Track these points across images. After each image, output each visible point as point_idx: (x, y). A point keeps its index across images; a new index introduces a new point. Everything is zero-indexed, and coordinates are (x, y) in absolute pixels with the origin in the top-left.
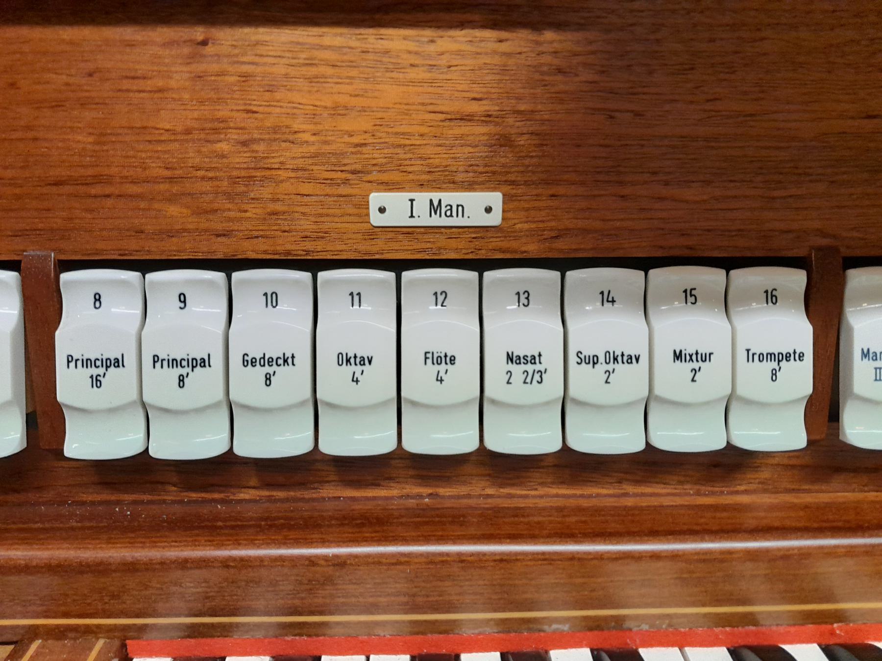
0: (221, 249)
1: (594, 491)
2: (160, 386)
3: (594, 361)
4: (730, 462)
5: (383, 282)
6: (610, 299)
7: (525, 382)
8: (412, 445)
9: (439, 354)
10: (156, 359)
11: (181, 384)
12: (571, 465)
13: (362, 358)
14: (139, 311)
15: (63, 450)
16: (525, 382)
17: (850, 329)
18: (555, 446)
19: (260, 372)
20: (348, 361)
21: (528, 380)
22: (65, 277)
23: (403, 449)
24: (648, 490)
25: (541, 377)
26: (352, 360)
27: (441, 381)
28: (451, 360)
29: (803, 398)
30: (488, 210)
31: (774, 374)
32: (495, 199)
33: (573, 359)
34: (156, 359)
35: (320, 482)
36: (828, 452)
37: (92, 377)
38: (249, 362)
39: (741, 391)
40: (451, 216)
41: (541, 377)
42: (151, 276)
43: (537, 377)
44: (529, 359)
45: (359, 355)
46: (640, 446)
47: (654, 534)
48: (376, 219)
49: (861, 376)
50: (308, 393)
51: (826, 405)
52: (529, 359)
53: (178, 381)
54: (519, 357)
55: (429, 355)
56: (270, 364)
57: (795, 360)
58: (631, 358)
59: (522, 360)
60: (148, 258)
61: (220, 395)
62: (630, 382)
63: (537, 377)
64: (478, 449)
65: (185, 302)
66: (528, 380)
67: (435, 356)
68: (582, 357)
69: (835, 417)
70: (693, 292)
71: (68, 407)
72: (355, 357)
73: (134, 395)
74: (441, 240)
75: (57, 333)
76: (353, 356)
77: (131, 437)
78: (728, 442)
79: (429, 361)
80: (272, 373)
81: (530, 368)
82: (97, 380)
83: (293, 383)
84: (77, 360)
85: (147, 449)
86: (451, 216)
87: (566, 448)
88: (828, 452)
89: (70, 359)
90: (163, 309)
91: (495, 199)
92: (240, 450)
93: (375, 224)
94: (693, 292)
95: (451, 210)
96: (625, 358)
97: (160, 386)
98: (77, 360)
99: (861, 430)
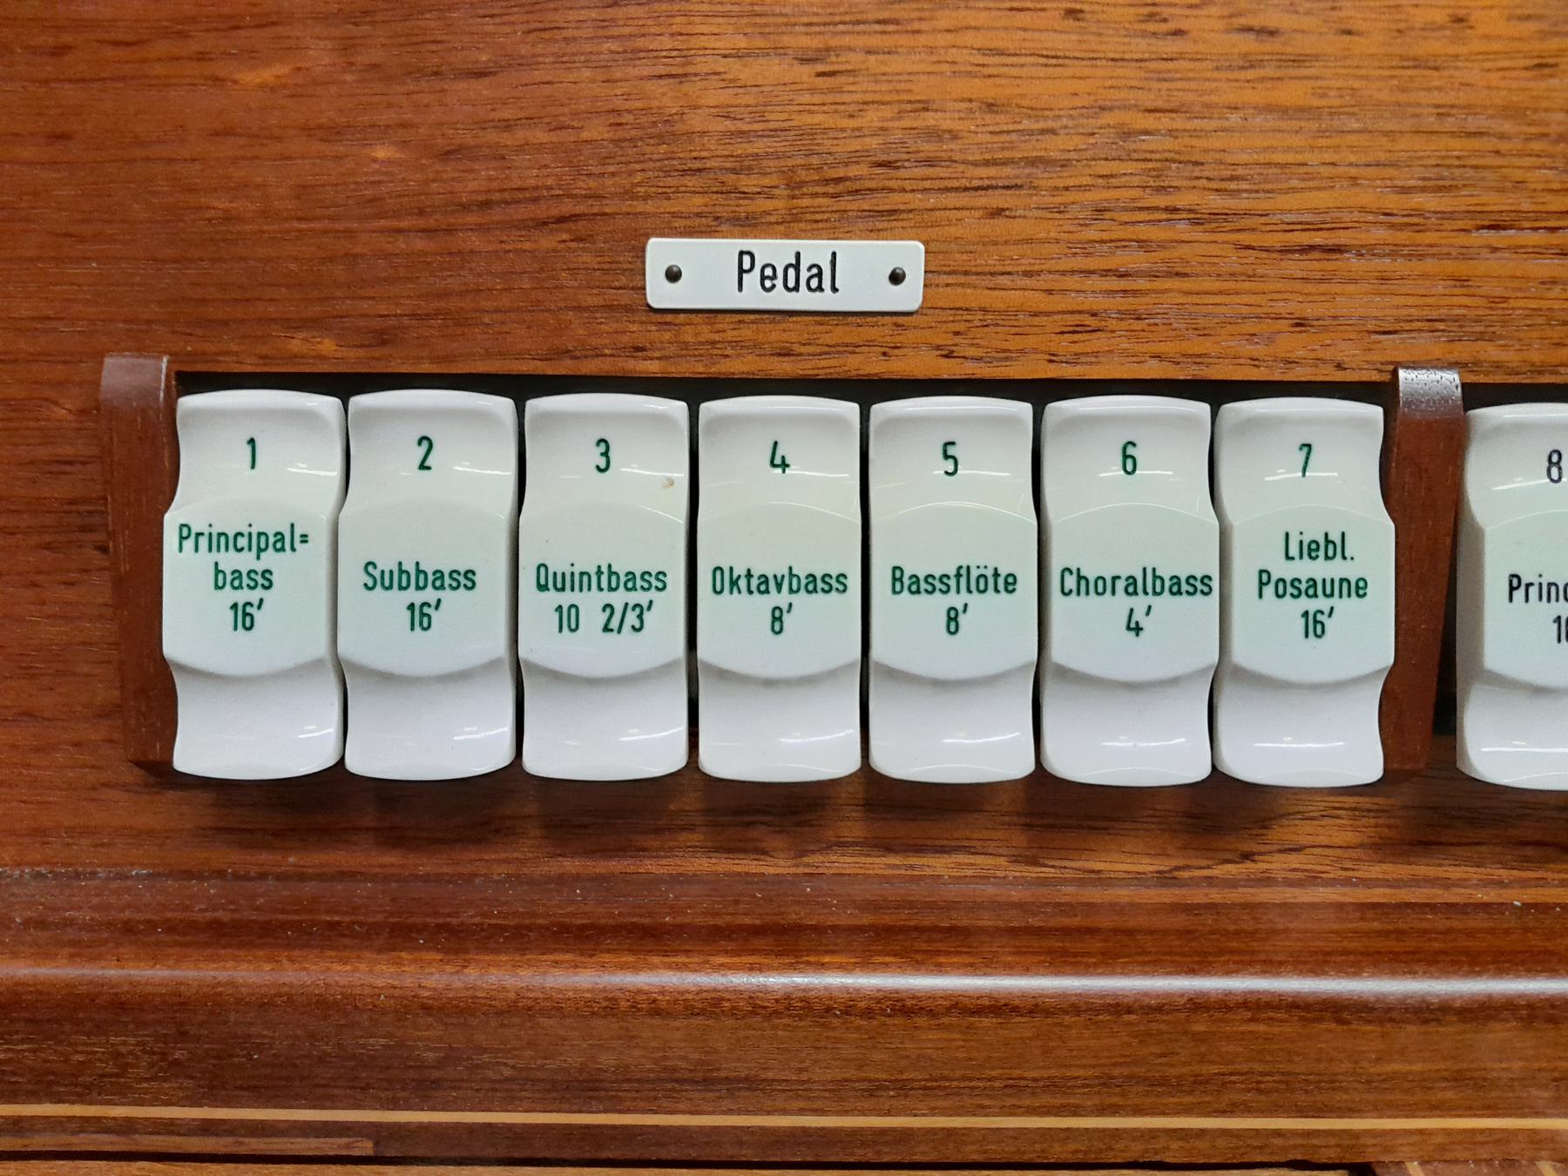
0: (328, 351)
1: (1455, 872)
2: (375, 631)
3: (1103, 586)
4: (1221, 810)
5: (1365, 422)
6: (778, 461)
7: (606, 629)
8: (720, 761)
9: (982, 571)
10: (1515, 583)
11: (953, 625)
12: (1051, 808)
13: (764, 579)
14: (336, 474)
15: (170, 762)
16: (606, 629)
17: (1478, 535)
18: (1020, 766)
19: (939, 604)
20: (734, 583)
21: (614, 624)
22: (188, 403)
23: (698, 769)
24: (1423, 870)
25: (640, 616)
26: (743, 583)
27: (1138, 629)
28: (1006, 583)
29: (1381, 671)
30: (673, 275)
31: (777, 617)
32: (910, 254)
33: (351, 576)
34: (1265, 577)
35: (658, 831)
36: (1428, 788)
37: (411, 607)
38: (377, 579)
39: (1241, 654)
40: (820, 288)
41: (640, 616)
42: (360, 401)
43: (631, 619)
44: (1303, 587)
45: (756, 573)
46: (1201, 771)
47: (1108, 961)
48: (660, 294)
49: (1508, 635)
50: (500, 647)
51: (1427, 689)
52: (1303, 587)
53: (770, 619)
54: (439, 574)
55: (963, 572)
56: (423, 587)
57: (997, 591)
58: (767, 582)
59: (820, 585)
60: (266, 369)
61: (498, 646)
62: (1183, 634)
63: (631, 619)
64: (860, 770)
65: (1126, 457)
66: (614, 624)
67: (974, 573)
68: (377, 574)
69: (1444, 718)
70: (951, 451)
71: (183, 668)
72: (749, 575)
73: (321, 648)
74: (791, 334)
75: (167, 516)
76: (743, 573)
77: (470, 734)
78: (1214, 767)
79: (1269, 591)
80: (960, 608)
81: (619, 599)
82: (1316, 622)
83: (826, 627)
84: (1528, 585)
85: (343, 758)
86: (820, 288)
87: (1041, 776)
88: (1428, 788)
89: (1515, 583)
90: (561, 469)
91: (910, 254)
92: (357, 764)
93: (655, 305)
94: (951, 451)
95: (820, 275)
96: (754, 582)
97: (375, 631)
98: (1528, 585)
99: (1506, 749)
